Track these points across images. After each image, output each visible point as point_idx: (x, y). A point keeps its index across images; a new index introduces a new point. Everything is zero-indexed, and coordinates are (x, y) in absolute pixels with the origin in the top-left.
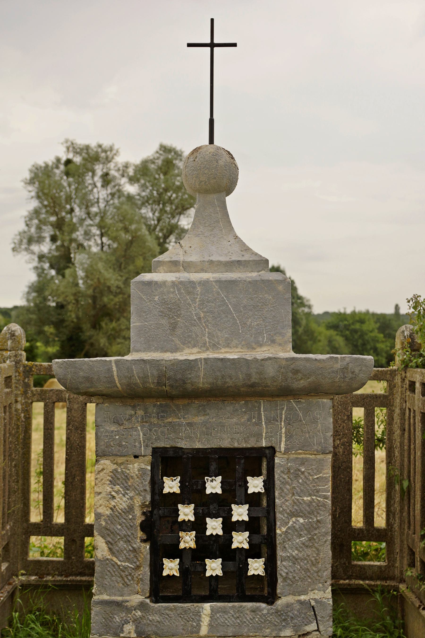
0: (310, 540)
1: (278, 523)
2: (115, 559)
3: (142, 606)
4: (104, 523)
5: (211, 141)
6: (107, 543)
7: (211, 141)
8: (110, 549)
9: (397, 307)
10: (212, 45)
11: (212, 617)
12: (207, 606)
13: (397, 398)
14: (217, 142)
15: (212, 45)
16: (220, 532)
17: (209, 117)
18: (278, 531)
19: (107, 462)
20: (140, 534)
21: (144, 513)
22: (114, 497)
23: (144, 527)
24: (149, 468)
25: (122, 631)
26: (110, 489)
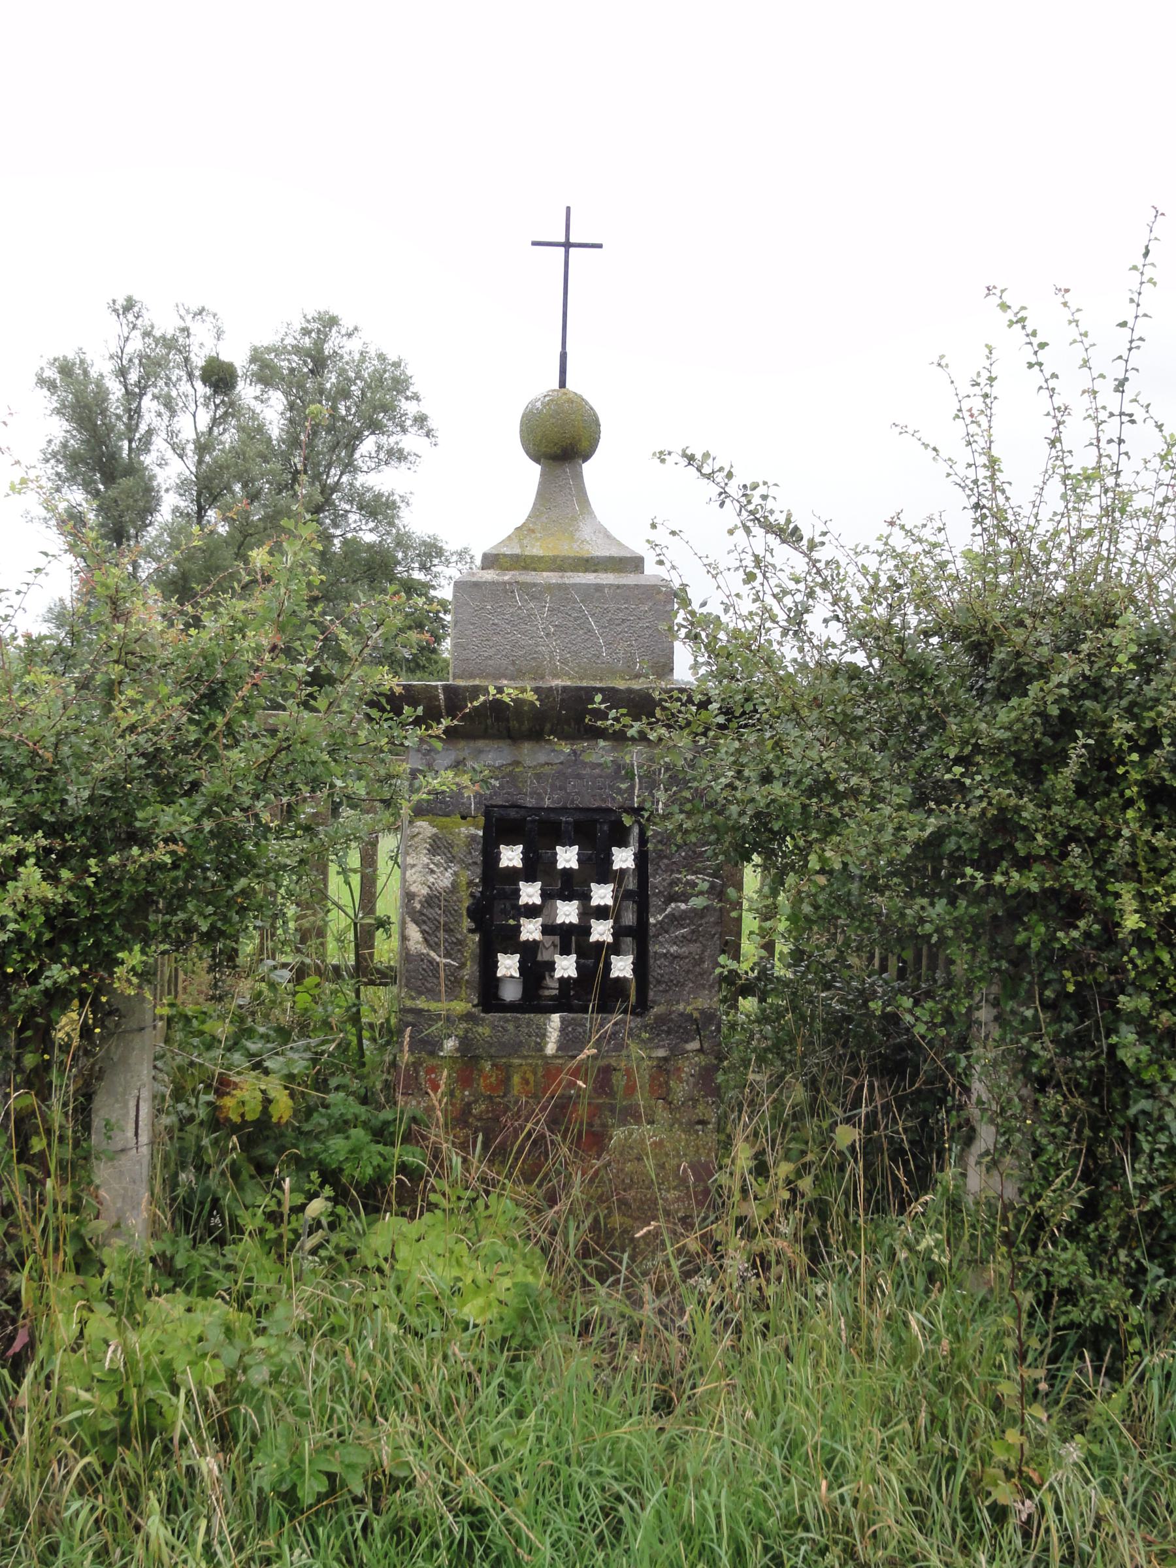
0: (693, 932)
1: (652, 910)
2: (432, 954)
3: (468, 1017)
4: (418, 906)
5: (563, 384)
6: (423, 932)
7: (563, 384)
8: (426, 940)
9: (416, 397)
10: (567, 245)
11: (562, 1030)
12: (556, 1018)
13: (1094, 1276)
14: (570, 385)
15: (567, 245)
16: (575, 920)
17: (560, 349)
18: (652, 920)
19: (425, 824)
20: (467, 923)
21: (472, 895)
22: (432, 872)
23: (472, 913)
24: (481, 833)
25: (441, 1049)
26: (426, 861)
